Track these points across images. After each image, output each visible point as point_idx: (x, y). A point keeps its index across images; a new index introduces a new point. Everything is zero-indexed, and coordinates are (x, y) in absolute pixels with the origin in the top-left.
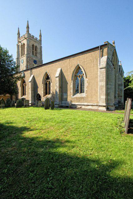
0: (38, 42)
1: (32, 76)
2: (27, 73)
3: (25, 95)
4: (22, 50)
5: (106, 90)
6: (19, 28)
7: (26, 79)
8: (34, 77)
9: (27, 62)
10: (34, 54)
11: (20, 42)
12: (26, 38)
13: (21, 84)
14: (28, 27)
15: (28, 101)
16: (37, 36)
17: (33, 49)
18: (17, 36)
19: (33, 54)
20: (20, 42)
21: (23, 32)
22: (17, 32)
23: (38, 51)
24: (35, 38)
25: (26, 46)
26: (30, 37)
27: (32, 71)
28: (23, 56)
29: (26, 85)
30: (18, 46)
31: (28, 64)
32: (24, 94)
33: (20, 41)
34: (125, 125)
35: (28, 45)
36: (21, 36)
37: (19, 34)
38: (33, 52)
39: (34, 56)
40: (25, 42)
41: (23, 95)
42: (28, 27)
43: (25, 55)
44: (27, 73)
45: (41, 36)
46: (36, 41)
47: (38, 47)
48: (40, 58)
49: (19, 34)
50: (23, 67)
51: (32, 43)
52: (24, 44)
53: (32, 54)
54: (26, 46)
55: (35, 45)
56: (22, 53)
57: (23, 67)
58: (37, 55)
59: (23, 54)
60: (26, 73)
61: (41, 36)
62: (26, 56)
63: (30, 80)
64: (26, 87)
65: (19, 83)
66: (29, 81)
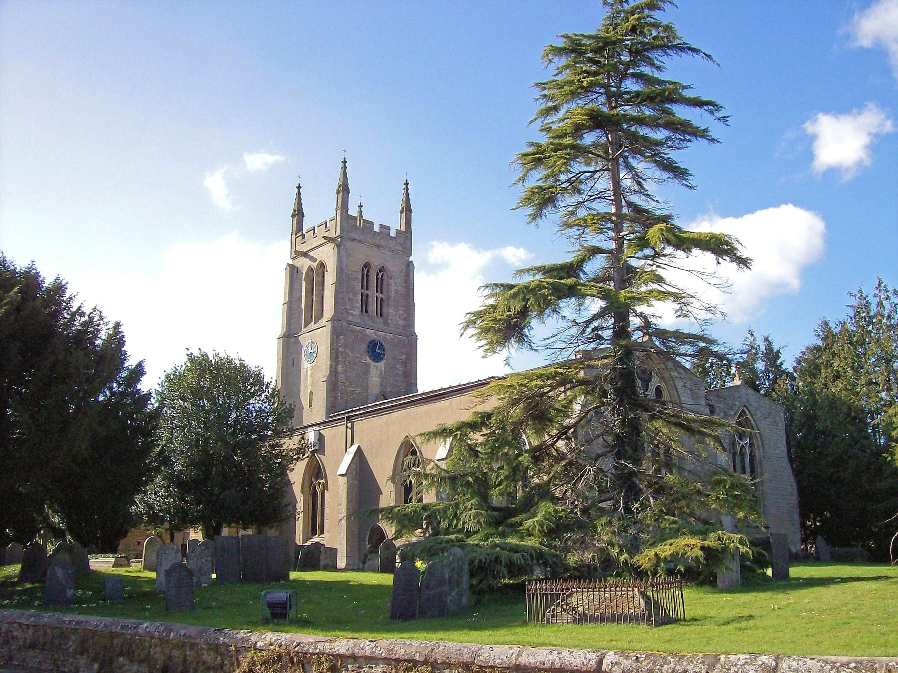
0: (392, 244)
1: (353, 449)
2: (334, 436)
3: (322, 532)
4: (310, 291)
5: (758, 590)
6: (299, 187)
7: (325, 460)
8: (359, 451)
9: (335, 355)
10: (372, 308)
11: (305, 255)
12: (329, 240)
13: (307, 484)
14: (344, 189)
15: (333, 552)
16: (383, 214)
17: (365, 285)
18: (288, 224)
19: (364, 309)
20: (305, 255)
21: (321, 210)
22: (291, 207)
23: (394, 286)
24: (376, 229)
25: (330, 279)
26: (353, 230)
27: (352, 429)
28: (312, 326)
29: (325, 487)
30: (293, 271)
31: (340, 368)
32: (315, 526)
33: (304, 249)
34: (37, 275)
35: (340, 271)
36: (306, 227)
37: (299, 213)
38: (365, 299)
39: (371, 318)
40: (328, 255)
41: (314, 533)
42: (344, 189)
43: (323, 321)
44: (335, 434)
45: (407, 209)
46: (382, 243)
47: (394, 267)
48: (401, 323)
49: (299, 213)
50: (313, 405)
51: (361, 254)
52: (322, 266)
53: (357, 312)
54: (330, 279)
55: (376, 263)
56: (309, 306)
57: (313, 405)
58: (385, 310)
59: (314, 314)
60: (327, 432)
61: (407, 209)
62: (329, 328)
63: (343, 469)
64: (327, 494)
65: (297, 474)
66: (339, 473)
